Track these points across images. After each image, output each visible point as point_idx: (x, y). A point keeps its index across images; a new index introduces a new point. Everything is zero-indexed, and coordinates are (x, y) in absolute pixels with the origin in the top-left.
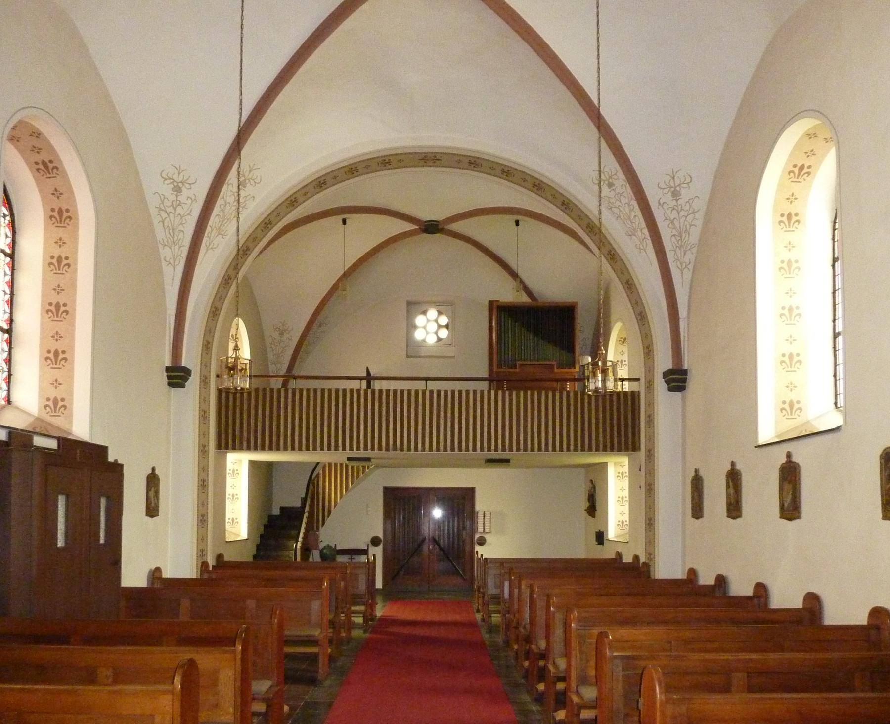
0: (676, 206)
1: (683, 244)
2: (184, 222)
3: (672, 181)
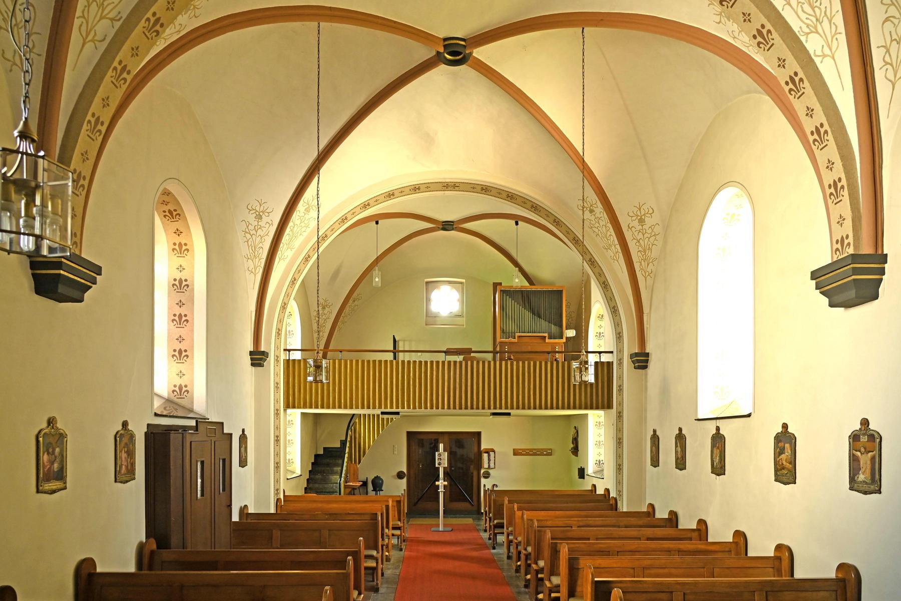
0: (642, 230)
1: (647, 258)
2: (263, 240)
3: (639, 211)
